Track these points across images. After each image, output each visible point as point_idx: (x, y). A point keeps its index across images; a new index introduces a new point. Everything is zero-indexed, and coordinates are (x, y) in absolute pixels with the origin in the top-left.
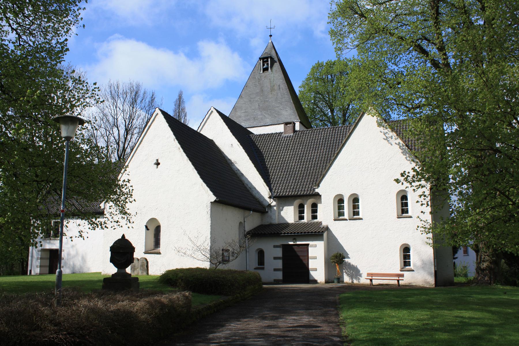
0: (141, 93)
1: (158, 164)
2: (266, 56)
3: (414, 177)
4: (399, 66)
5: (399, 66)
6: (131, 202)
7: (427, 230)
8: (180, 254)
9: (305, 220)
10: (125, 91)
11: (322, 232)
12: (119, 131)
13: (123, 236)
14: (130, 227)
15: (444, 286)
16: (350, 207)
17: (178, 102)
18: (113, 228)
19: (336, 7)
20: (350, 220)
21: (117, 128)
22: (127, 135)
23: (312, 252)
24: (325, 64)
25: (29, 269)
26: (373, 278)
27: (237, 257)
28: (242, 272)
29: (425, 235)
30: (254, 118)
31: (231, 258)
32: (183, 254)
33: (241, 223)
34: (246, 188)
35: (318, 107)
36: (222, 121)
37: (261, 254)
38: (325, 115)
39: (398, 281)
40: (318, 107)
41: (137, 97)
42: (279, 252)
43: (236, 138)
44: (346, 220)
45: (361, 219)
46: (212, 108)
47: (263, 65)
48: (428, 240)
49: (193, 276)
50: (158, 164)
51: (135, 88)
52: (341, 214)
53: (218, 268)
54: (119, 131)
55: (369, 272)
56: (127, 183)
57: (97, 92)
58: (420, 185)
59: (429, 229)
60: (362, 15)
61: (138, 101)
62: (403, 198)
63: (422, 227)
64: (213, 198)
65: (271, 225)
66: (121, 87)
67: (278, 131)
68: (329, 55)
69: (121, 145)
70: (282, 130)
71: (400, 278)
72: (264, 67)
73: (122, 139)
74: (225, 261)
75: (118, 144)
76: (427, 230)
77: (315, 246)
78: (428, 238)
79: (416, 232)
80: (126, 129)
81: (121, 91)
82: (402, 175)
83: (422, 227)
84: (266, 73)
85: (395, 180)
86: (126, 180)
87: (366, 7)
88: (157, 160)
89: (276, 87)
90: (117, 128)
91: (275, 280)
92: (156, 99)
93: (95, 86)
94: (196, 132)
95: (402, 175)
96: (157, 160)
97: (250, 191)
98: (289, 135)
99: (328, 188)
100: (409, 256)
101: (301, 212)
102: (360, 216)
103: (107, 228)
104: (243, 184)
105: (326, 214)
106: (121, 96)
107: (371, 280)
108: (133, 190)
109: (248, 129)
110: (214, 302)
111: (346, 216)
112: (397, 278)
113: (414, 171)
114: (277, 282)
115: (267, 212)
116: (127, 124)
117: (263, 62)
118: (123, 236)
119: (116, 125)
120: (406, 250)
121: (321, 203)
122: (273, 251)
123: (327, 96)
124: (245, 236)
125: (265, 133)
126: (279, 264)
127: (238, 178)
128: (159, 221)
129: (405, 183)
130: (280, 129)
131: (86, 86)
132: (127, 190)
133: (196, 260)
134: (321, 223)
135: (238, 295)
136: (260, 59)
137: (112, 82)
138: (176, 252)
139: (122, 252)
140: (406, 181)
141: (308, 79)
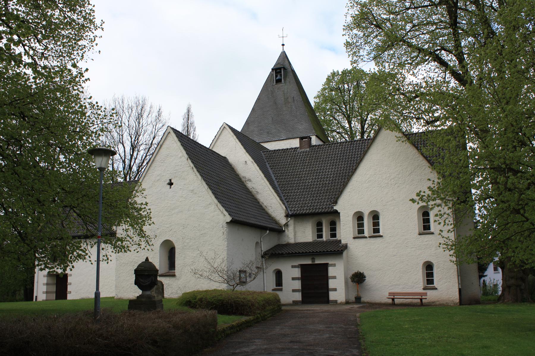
0: (147, 108)
1: (171, 184)
2: (278, 66)
3: (429, 196)
4: (418, 77)
5: (418, 77)
6: (150, 225)
7: (449, 247)
8: (197, 276)
9: (324, 239)
10: (130, 106)
11: (342, 250)
12: (124, 147)
13: (147, 259)
14: (150, 250)
15: (469, 304)
16: (370, 224)
17: (187, 116)
18: (136, 251)
19: (351, 19)
20: (370, 237)
21: (123, 144)
22: (133, 152)
23: (332, 271)
24: (340, 73)
25: (35, 295)
26: (395, 297)
27: (254, 279)
28: (261, 292)
29: (447, 252)
30: (268, 133)
31: (248, 279)
32: (199, 276)
33: (257, 243)
34: (261, 206)
35: (335, 119)
36: (235, 137)
37: (279, 274)
38: (343, 127)
39: (421, 299)
40: (335, 119)
41: (143, 112)
42: (297, 272)
43: (250, 154)
44: (366, 237)
45: (382, 236)
46: (225, 124)
47: (276, 76)
48: (451, 258)
49: (213, 298)
50: (171, 184)
51: (141, 102)
52: (361, 232)
53: (235, 289)
54: (124, 147)
55: (390, 291)
56: (145, 206)
57: (115, 117)
58: (435, 204)
59: (452, 246)
60: (378, 26)
61: (145, 116)
62: (425, 215)
63: (445, 244)
64: (229, 219)
65: (288, 245)
66: (126, 102)
67: (294, 146)
68: (343, 63)
69: (127, 162)
70: (298, 145)
71: (423, 297)
72: (277, 78)
73: (128, 157)
74: (243, 283)
75: (124, 162)
76: (449, 247)
77: (334, 265)
78: (450, 256)
79: (437, 248)
80: (132, 145)
81: (126, 106)
82: (418, 195)
83: (445, 244)
84: (280, 85)
85: (411, 200)
86: (144, 203)
87: (382, 16)
88: (170, 180)
89: (290, 100)
90: (123, 144)
91: (293, 301)
92: (163, 114)
93: (113, 112)
94: (208, 149)
95: (418, 195)
96: (170, 180)
97: (266, 209)
98: (305, 150)
99: (348, 205)
100: (432, 274)
101: (320, 230)
102: (381, 234)
103: (130, 251)
104: (259, 203)
105: (346, 231)
106: (126, 110)
107: (393, 299)
108: (151, 212)
109: (262, 144)
110: (237, 322)
111: (366, 234)
112: (420, 297)
113: (430, 190)
114: (295, 303)
115: (284, 231)
116: (133, 140)
117: (276, 73)
118: (147, 259)
119: (121, 141)
120: (429, 267)
121: (347, 69)
122: (291, 272)
123: (344, 106)
124: (262, 257)
125: (280, 149)
126: (298, 285)
127: (253, 196)
128: (174, 242)
129: (420, 202)
130: (295, 143)
131: (104, 111)
132: (145, 213)
133: (213, 283)
134: (340, 241)
135: (258, 315)
136: (273, 69)
137: (116, 96)
138: (192, 274)
139: (146, 275)
140: (421, 200)
141: (324, 89)
